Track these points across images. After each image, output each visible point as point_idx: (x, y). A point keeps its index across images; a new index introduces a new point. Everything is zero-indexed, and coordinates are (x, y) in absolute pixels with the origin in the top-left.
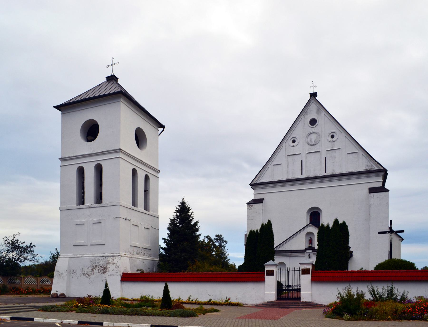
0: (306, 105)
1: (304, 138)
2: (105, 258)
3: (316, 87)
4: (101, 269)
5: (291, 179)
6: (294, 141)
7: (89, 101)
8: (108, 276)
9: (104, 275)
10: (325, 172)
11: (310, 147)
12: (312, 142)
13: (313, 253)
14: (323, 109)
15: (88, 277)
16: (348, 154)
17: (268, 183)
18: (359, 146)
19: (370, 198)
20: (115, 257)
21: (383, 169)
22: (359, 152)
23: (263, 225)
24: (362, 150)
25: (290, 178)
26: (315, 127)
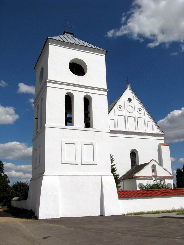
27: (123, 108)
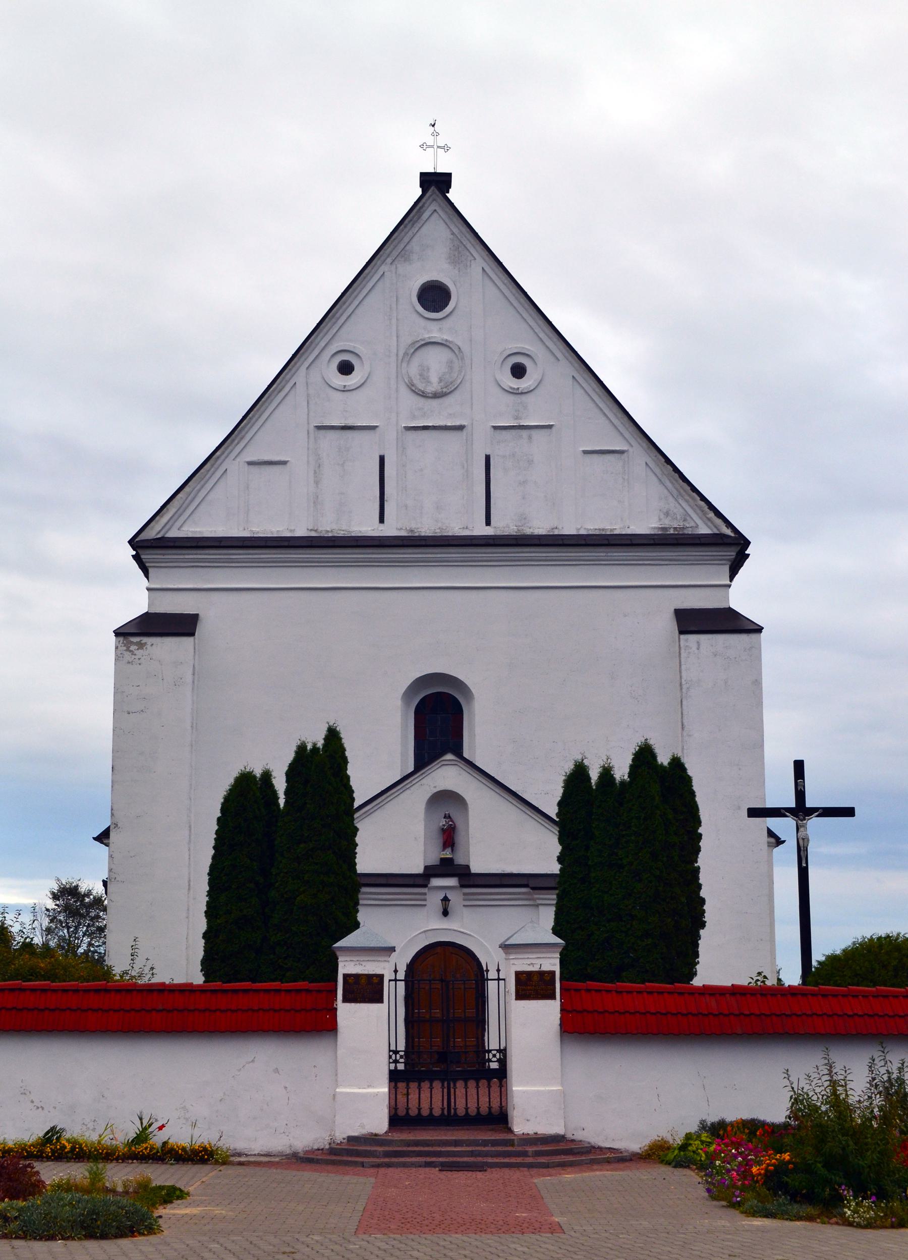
0: (406, 222)
1: (394, 359)
3: (446, 148)
5: (330, 535)
6: (346, 368)
10: (488, 523)
11: (421, 402)
12: (427, 381)
13: (465, 894)
14: (479, 247)
16: (586, 452)
17: (223, 544)
18: (634, 428)
19: (683, 655)
21: (733, 535)
22: (631, 450)
23: (301, 749)
24: (644, 445)
25: (328, 531)
26: (447, 316)
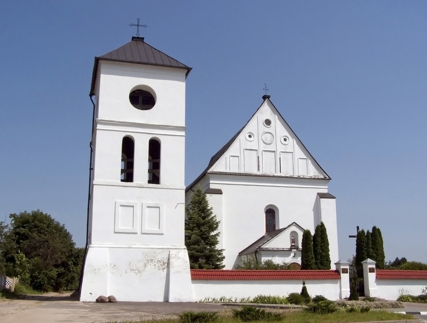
2: (165, 250)
4: (159, 264)
7: (152, 66)
8: (173, 274)
9: (163, 272)
15: (139, 274)
20: (180, 250)
27: (256, 136)
